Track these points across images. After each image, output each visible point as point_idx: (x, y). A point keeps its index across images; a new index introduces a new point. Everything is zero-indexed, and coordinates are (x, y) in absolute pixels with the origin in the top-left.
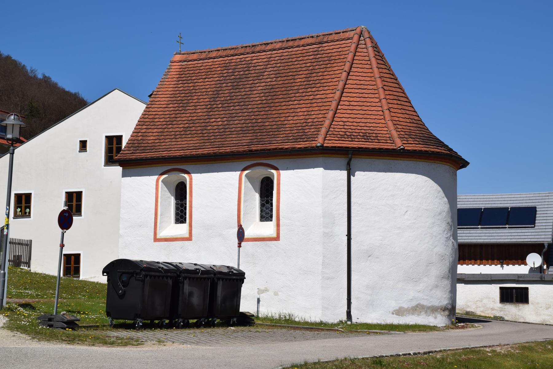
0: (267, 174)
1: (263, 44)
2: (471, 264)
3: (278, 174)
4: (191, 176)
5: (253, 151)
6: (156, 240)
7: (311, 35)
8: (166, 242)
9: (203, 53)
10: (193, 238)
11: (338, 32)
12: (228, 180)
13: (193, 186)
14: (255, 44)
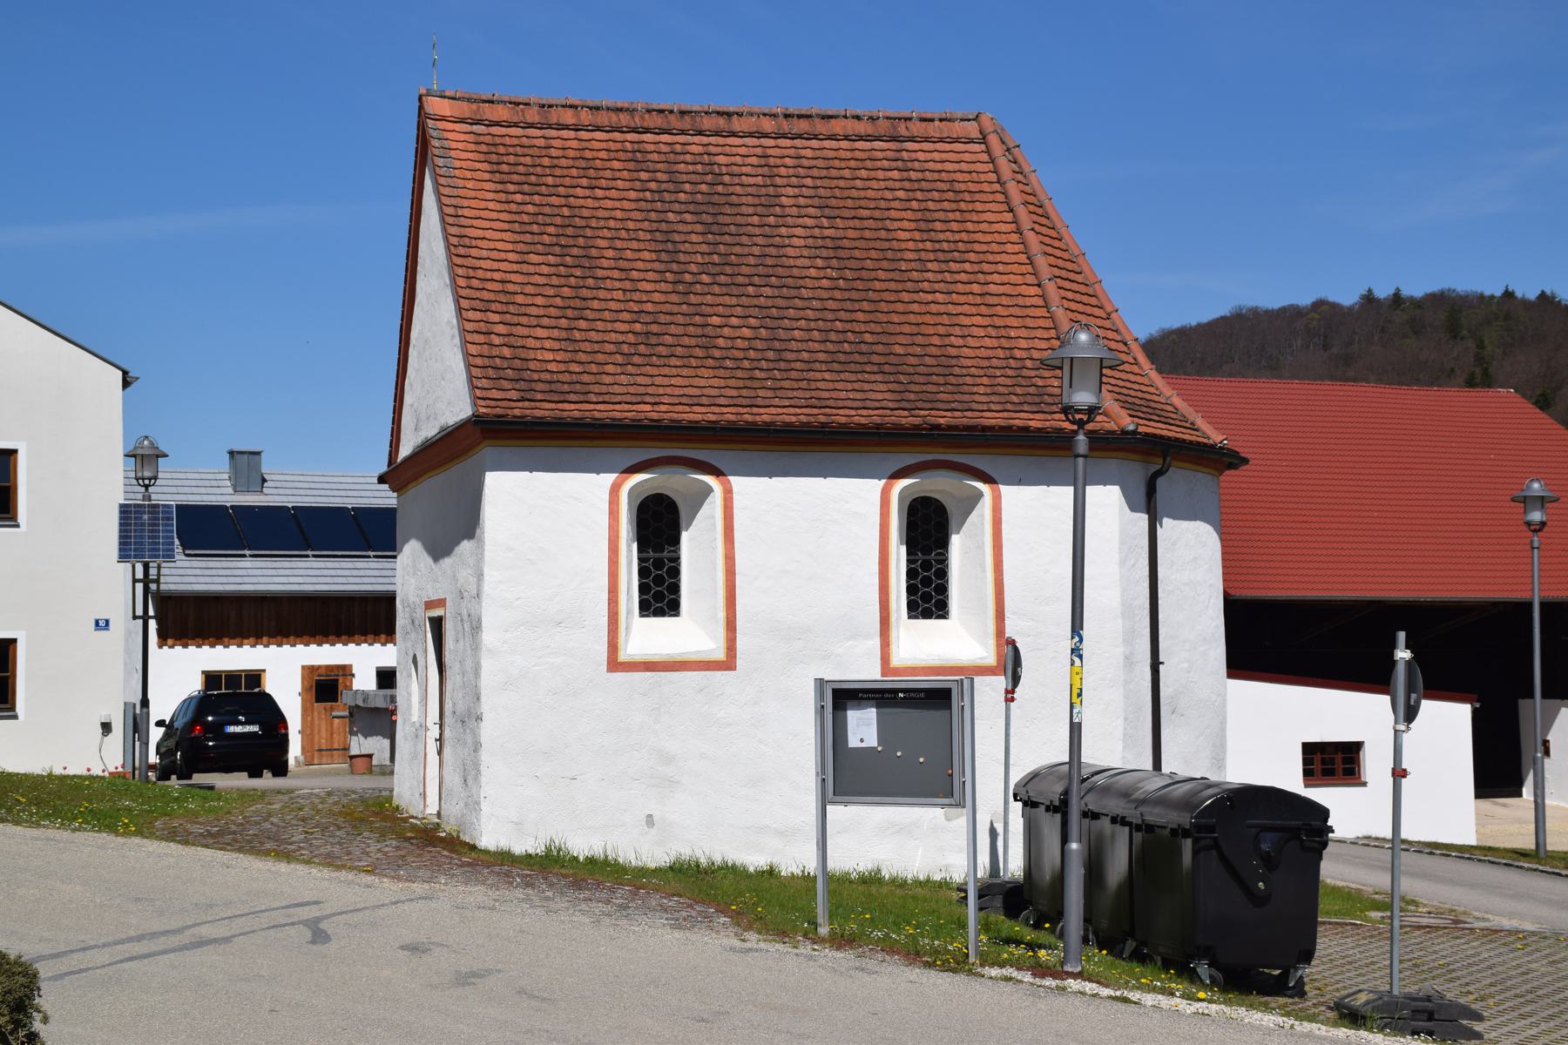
0: (924, 491)
1: (713, 112)
2: (365, 642)
3: (996, 493)
4: (729, 481)
5: (943, 429)
6: (614, 665)
7: (854, 113)
8: (649, 673)
9: (521, 106)
10: (739, 662)
11: (929, 116)
12: (847, 502)
13: (735, 511)
14: (689, 109)
